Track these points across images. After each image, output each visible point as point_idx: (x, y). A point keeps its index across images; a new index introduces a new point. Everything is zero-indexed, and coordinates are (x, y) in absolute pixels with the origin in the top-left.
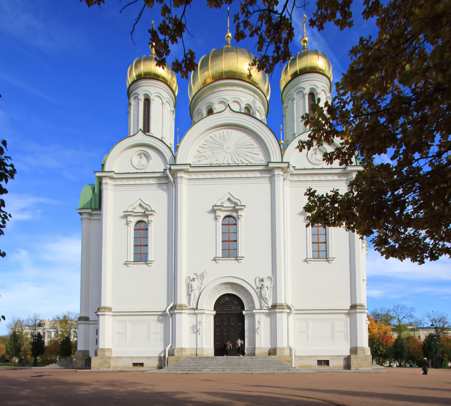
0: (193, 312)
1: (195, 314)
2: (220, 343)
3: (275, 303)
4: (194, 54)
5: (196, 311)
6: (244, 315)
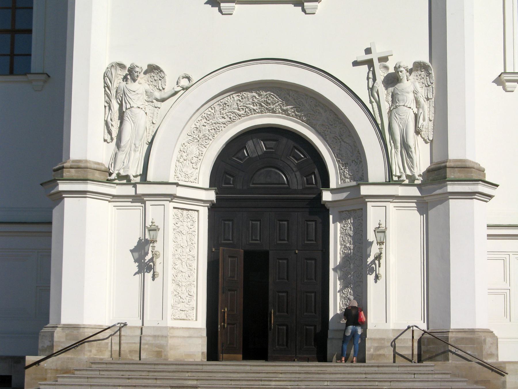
0: (129, 190)
1: (139, 199)
2: (233, 240)
3: (443, 159)
4: (222, 15)
5: (142, 189)
6: (328, 206)
